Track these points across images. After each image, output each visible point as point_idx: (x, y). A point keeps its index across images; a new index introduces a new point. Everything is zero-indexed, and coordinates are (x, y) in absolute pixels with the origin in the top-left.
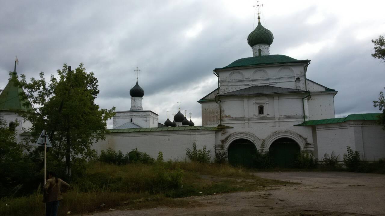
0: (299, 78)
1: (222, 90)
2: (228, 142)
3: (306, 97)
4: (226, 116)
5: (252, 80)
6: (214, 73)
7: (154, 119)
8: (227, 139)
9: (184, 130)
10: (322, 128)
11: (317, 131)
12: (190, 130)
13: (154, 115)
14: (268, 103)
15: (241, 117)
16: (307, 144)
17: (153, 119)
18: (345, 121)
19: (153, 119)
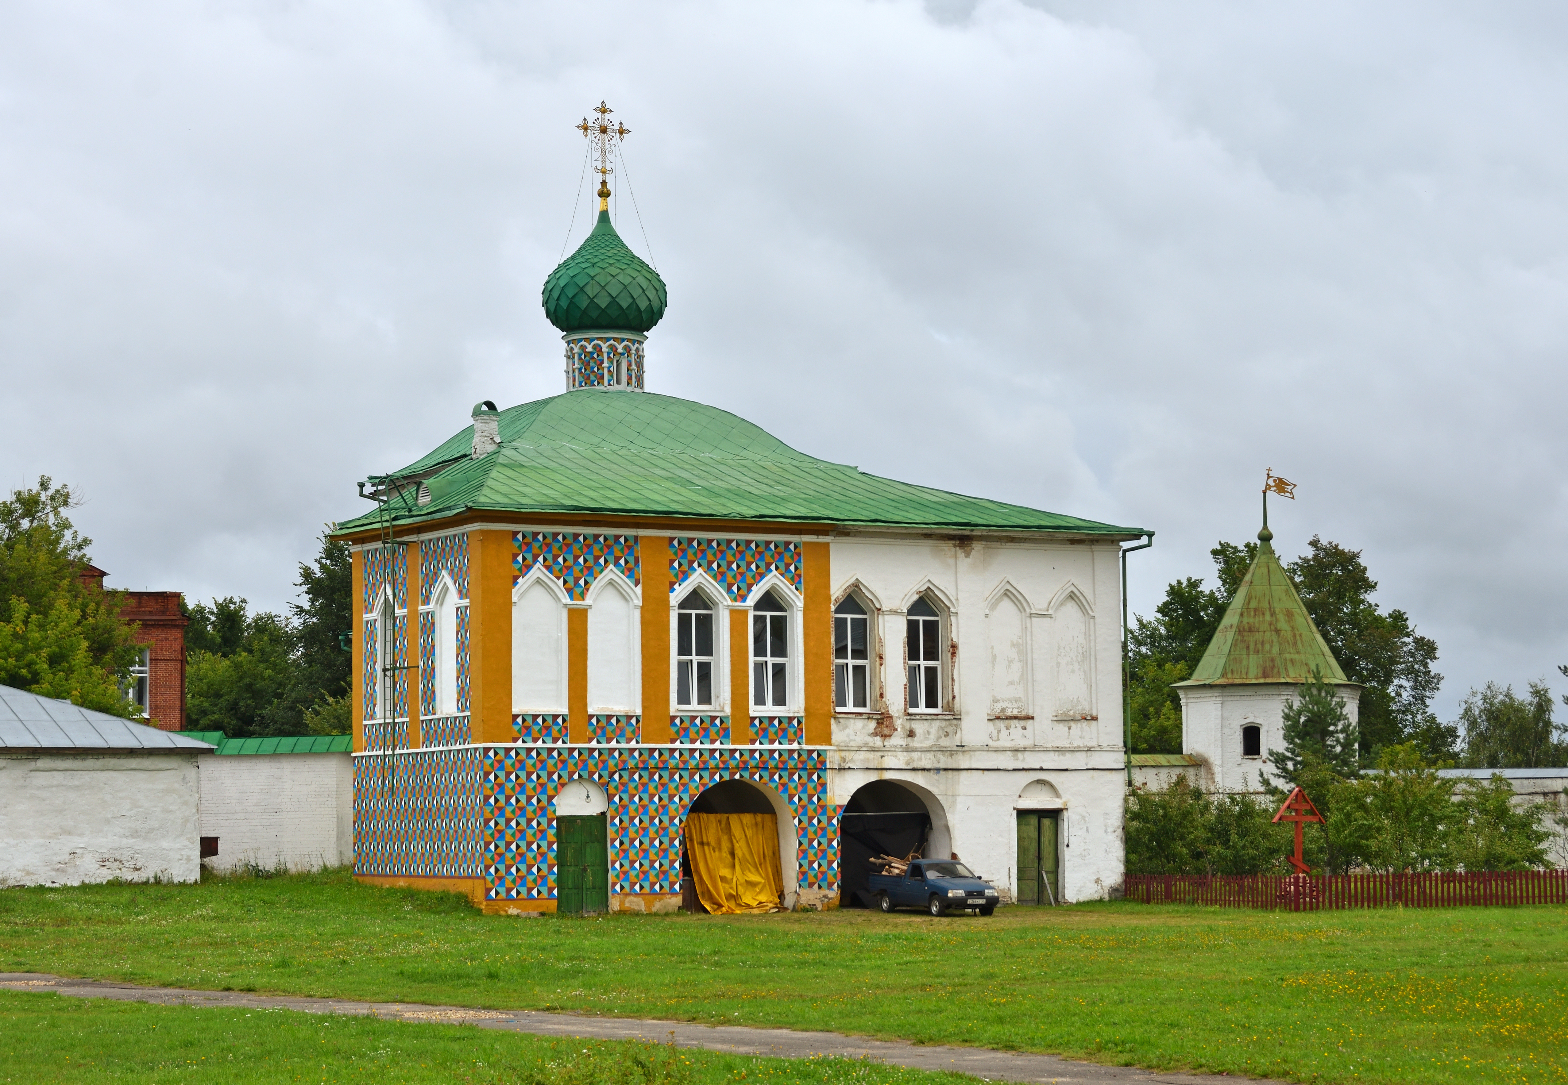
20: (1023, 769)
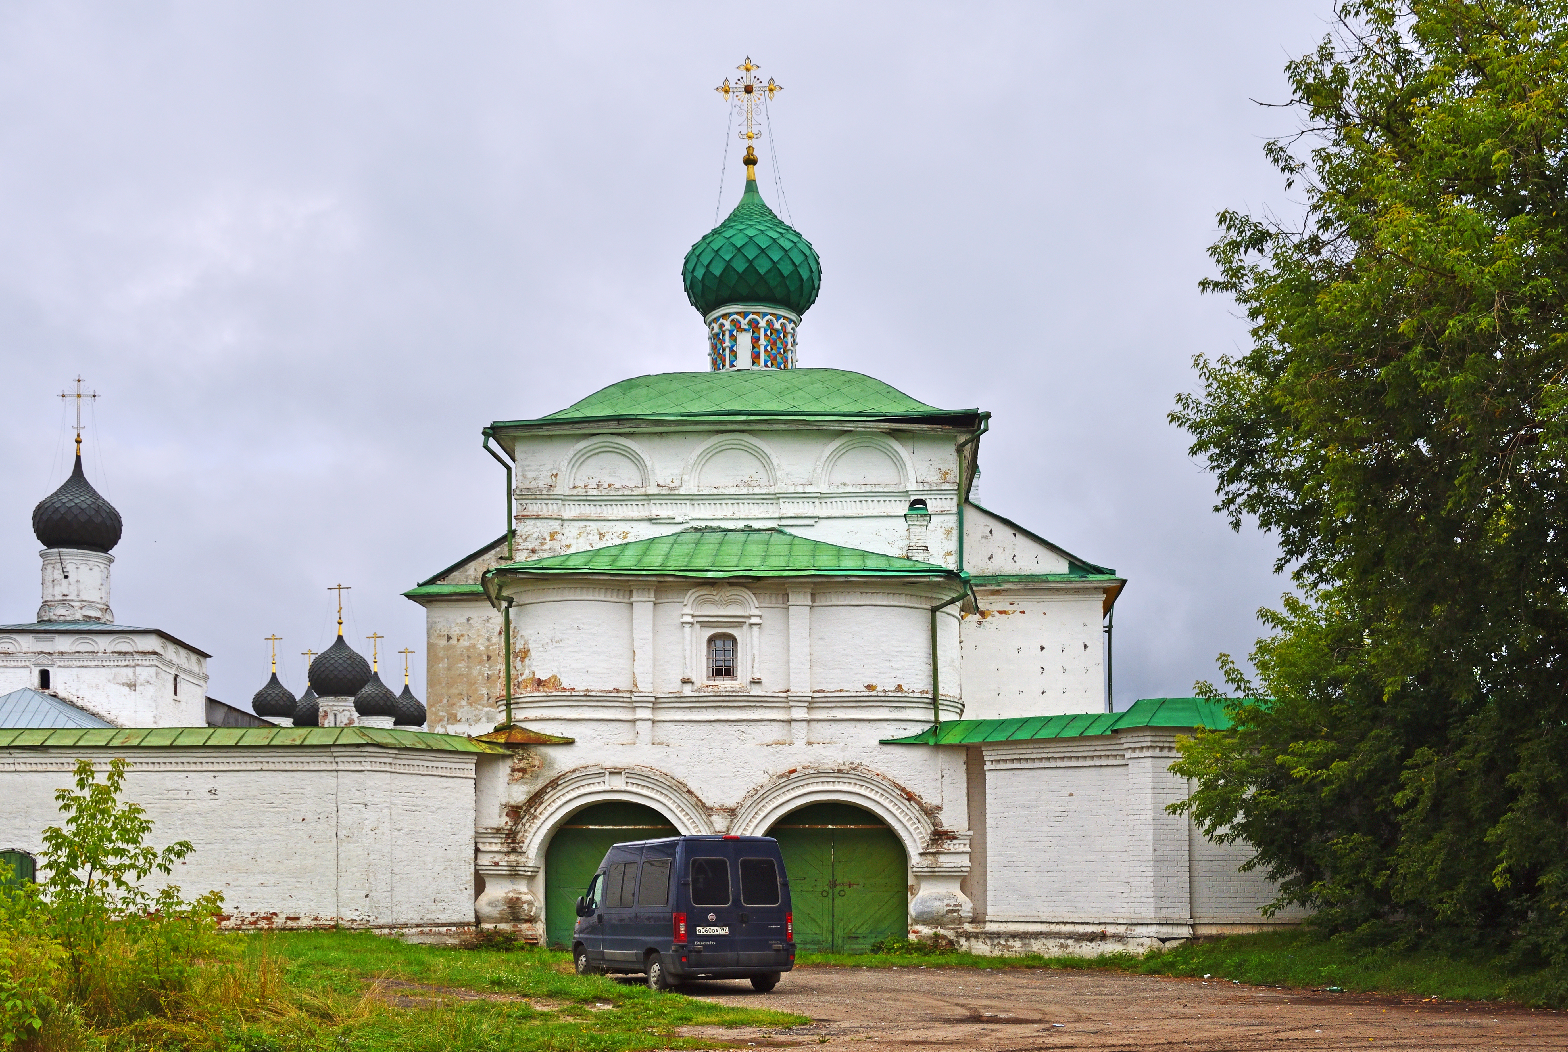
0: (923, 502)
1: (525, 540)
2: (543, 818)
3: (952, 601)
4: (539, 682)
5: (692, 498)
6: (486, 447)
7: (182, 675)
8: (536, 799)
9: (301, 746)
10: (1013, 760)
11: (988, 775)
12: (334, 745)
13: (183, 653)
14: (760, 624)
15: (618, 691)
16: (940, 836)
17: (176, 677)
18: (1115, 732)
19: (176, 677)
20: (844, 517)
